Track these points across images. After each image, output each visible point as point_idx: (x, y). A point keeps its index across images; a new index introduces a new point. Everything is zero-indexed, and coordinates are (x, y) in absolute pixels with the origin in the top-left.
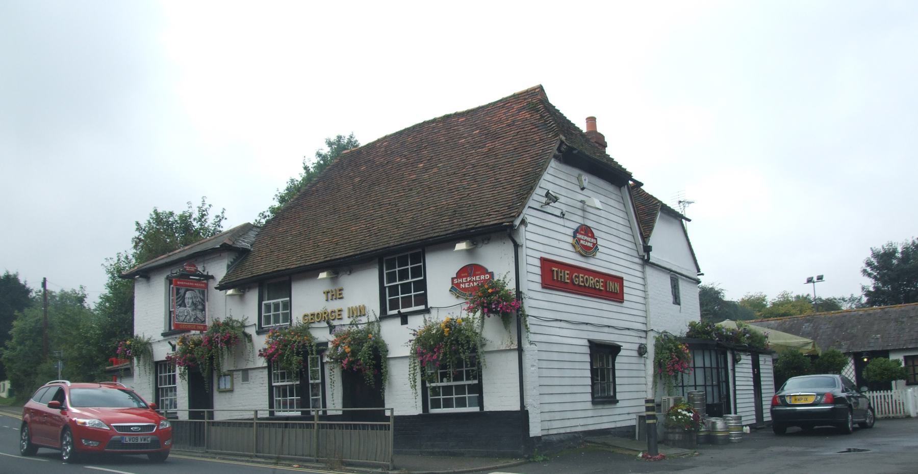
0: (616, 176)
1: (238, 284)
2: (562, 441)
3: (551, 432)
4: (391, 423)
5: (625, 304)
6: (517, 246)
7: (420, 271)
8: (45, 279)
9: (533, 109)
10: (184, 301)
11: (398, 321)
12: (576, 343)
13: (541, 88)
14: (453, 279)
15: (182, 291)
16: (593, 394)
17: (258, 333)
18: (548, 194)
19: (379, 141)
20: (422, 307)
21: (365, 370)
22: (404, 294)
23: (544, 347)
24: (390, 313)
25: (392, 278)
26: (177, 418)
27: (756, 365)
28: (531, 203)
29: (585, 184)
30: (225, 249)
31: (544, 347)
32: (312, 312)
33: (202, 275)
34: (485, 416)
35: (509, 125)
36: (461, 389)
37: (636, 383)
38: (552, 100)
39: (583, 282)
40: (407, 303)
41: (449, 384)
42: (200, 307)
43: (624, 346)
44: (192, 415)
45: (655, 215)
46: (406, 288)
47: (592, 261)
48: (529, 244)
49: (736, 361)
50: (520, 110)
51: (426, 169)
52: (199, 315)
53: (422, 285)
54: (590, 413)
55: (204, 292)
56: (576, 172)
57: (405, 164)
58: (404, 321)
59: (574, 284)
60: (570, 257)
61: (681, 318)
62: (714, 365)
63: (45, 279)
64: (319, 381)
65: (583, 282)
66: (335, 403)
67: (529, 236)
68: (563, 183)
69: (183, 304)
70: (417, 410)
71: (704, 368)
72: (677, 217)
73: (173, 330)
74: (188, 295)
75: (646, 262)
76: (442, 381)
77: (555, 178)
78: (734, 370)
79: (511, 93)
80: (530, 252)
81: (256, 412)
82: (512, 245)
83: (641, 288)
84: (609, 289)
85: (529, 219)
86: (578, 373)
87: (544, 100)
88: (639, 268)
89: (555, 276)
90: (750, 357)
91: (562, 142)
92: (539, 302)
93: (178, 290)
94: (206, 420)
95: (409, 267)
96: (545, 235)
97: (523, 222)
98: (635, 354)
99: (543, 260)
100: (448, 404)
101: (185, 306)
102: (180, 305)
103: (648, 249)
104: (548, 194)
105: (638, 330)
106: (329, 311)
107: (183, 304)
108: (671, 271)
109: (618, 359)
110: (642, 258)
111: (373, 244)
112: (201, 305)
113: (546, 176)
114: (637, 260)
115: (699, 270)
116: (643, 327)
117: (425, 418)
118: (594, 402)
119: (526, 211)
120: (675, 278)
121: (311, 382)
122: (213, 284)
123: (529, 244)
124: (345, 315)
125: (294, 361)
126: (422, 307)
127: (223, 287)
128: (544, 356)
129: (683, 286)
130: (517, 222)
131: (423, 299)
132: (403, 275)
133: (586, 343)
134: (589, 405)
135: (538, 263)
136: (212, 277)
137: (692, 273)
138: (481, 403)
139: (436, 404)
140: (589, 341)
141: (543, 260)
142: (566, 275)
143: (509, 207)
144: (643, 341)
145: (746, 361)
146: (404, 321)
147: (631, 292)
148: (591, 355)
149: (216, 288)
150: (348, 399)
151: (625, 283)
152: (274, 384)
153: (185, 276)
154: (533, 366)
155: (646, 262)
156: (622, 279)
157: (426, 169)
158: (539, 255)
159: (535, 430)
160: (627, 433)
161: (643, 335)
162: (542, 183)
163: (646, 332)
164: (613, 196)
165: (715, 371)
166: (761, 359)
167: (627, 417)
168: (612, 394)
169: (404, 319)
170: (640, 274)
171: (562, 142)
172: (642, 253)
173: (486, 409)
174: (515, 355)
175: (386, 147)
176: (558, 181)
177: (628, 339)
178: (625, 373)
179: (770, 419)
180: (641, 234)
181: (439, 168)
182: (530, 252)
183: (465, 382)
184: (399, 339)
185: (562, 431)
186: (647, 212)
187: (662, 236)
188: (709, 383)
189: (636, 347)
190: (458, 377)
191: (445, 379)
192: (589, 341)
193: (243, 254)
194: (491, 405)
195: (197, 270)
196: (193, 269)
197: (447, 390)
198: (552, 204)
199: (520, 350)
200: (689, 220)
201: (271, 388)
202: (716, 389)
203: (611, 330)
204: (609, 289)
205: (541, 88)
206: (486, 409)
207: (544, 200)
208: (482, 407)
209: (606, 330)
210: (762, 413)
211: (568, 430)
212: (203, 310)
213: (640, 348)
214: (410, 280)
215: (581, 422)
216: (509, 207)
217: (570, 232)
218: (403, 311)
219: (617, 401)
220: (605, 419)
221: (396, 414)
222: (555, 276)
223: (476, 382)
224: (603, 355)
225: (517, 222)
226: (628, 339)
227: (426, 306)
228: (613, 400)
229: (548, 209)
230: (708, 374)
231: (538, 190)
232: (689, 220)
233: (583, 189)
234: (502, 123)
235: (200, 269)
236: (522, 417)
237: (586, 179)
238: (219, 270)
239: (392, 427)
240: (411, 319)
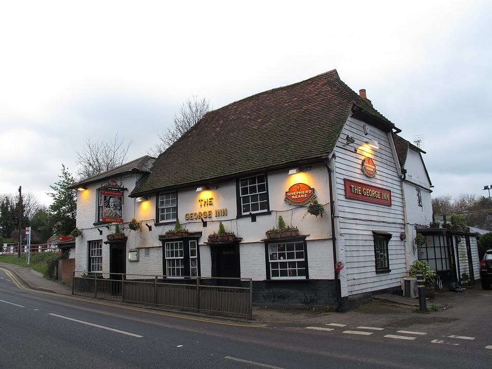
0: (384, 126)
1: (142, 193)
2: (360, 299)
3: (353, 293)
4: (251, 288)
5: (392, 207)
6: (330, 172)
7: (264, 188)
8: (20, 187)
9: (330, 83)
10: (109, 204)
11: (250, 219)
12: (364, 233)
13: (335, 71)
14: (286, 192)
15: (108, 198)
16: (376, 267)
17: (156, 225)
18: (348, 138)
19: (229, 105)
20: (266, 211)
21: (226, 250)
22: (253, 201)
23: (347, 237)
24: (244, 214)
25: (245, 191)
26: (102, 277)
27: (468, 244)
28: (338, 144)
29: (368, 131)
30: (135, 172)
31: (347, 237)
32: (191, 212)
33: (121, 188)
34: (309, 283)
35: (317, 95)
36: (292, 264)
37: (402, 258)
38: (343, 78)
39: (368, 194)
40: (255, 207)
41: (285, 261)
42: (119, 208)
43: (394, 234)
44: (112, 277)
45: (407, 150)
46: (254, 198)
47: (373, 180)
48: (338, 170)
49: (457, 242)
50: (323, 85)
51: (263, 123)
52: (118, 212)
53: (266, 196)
54: (375, 279)
55: (121, 198)
56: (362, 124)
57: (249, 119)
58: (254, 220)
59: (363, 195)
60: (358, 177)
61: (425, 217)
62: (446, 245)
63: (20, 187)
64: (196, 257)
65: (368, 194)
66: (206, 271)
67: (337, 165)
68: (355, 131)
69: (108, 206)
70: (263, 278)
71: (440, 247)
72: (418, 151)
73: (101, 222)
74: (111, 200)
75: (403, 180)
76: (279, 259)
77: (351, 127)
78: (457, 248)
79: (316, 75)
80: (338, 175)
81: (157, 277)
82: (326, 169)
83: (400, 196)
84: (382, 198)
85: (337, 154)
86: (367, 254)
87: (338, 79)
88: (398, 183)
89: (354, 191)
90: (464, 239)
91: (354, 105)
92: (345, 207)
93: (105, 197)
94: (123, 281)
95: (257, 184)
96: (346, 165)
97: (334, 156)
98: (399, 239)
99: (345, 180)
100: (284, 274)
101: (110, 207)
102: (107, 207)
103: (404, 172)
104: (348, 138)
105: (400, 224)
106: (203, 212)
107: (108, 206)
108: (417, 185)
109: (390, 243)
110: (400, 177)
111: (234, 171)
112: (119, 206)
113: (345, 126)
114: (397, 179)
115: (431, 184)
116: (401, 221)
117: (268, 283)
118: (377, 272)
119: (335, 149)
120: (418, 187)
121: (191, 257)
122: (127, 194)
123: (338, 170)
124: (214, 215)
125: (180, 243)
126: (266, 211)
127: (134, 195)
128: (348, 243)
129: (423, 194)
130: (330, 156)
131: (266, 205)
132: (253, 189)
133: (371, 233)
134: (374, 274)
135: (342, 182)
136: (126, 189)
137: (427, 186)
138: (306, 273)
139: (276, 274)
140: (373, 232)
141: (345, 180)
142: (358, 190)
143: (324, 147)
144: (403, 231)
145: (463, 240)
146: (254, 220)
147: (396, 201)
148: (375, 241)
149: (129, 196)
150: (216, 269)
151: (392, 194)
152: (166, 258)
153: (106, 189)
154: (342, 250)
155: (403, 180)
156: (390, 191)
157: (263, 123)
158: (343, 177)
159: (344, 293)
160: (396, 291)
161: (403, 227)
162: (344, 131)
163: (404, 225)
164: (383, 139)
165: (446, 249)
166: (470, 239)
167: (394, 281)
168: (387, 266)
169: (253, 218)
170: (399, 188)
171: (354, 105)
172: (400, 174)
173: (311, 278)
174: (331, 243)
175: (235, 109)
176: (353, 130)
177: (394, 230)
178: (394, 252)
179: (479, 278)
180: (400, 162)
181: (272, 122)
182: (338, 175)
183: (295, 260)
184: (252, 232)
185: (360, 292)
186: (402, 149)
187: (411, 163)
188: (443, 257)
189: (399, 235)
190: (291, 256)
191: (282, 258)
192: (373, 232)
193: (146, 174)
194: (313, 275)
195: (117, 185)
196: (114, 184)
197: (283, 265)
198: (351, 144)
199: (334, 239)
200: (425, 153)
201: (164, 260)
202: (448, 260)
203: (385, 224)
204: (382, 198)
205: (335, 71)
206: (311, 278)
207: (345, 142)
208: (307, 277)
209: (382, 224)
210: (473, 275)
211: (364, 291)
212: (121, 209)
213: (401, 235)
214: (257, 193)
215: (370, 285)
216: (324, 147)
217: (360, 162)
218: (253, 213)
219: (390, 271)
220: (384, 283)
221: (253, 280)
222: (354, 191)
223: (303, 260)
224: (381, 240)
225: (330, 156)
226: (394, 230)
227: (269, 209)
228: (388, 270)
229: (347, 147)
230: (443, 250)
231: (342, 136)
232: (425, 153)
233: (366, 134)
234: (312, 93)
235: (119, 184)
236: (336, 284)
237: (369, 128)
238: (130, 185)
239: (251, 292)
240: (258, 218)
